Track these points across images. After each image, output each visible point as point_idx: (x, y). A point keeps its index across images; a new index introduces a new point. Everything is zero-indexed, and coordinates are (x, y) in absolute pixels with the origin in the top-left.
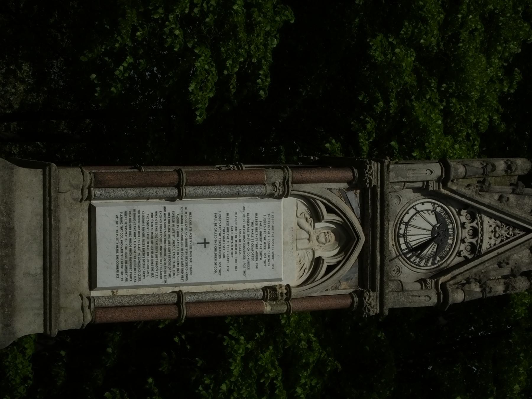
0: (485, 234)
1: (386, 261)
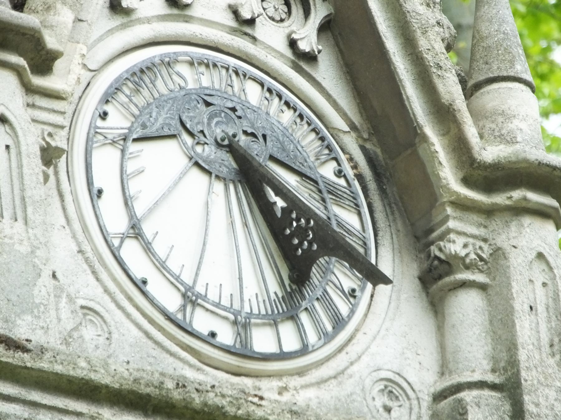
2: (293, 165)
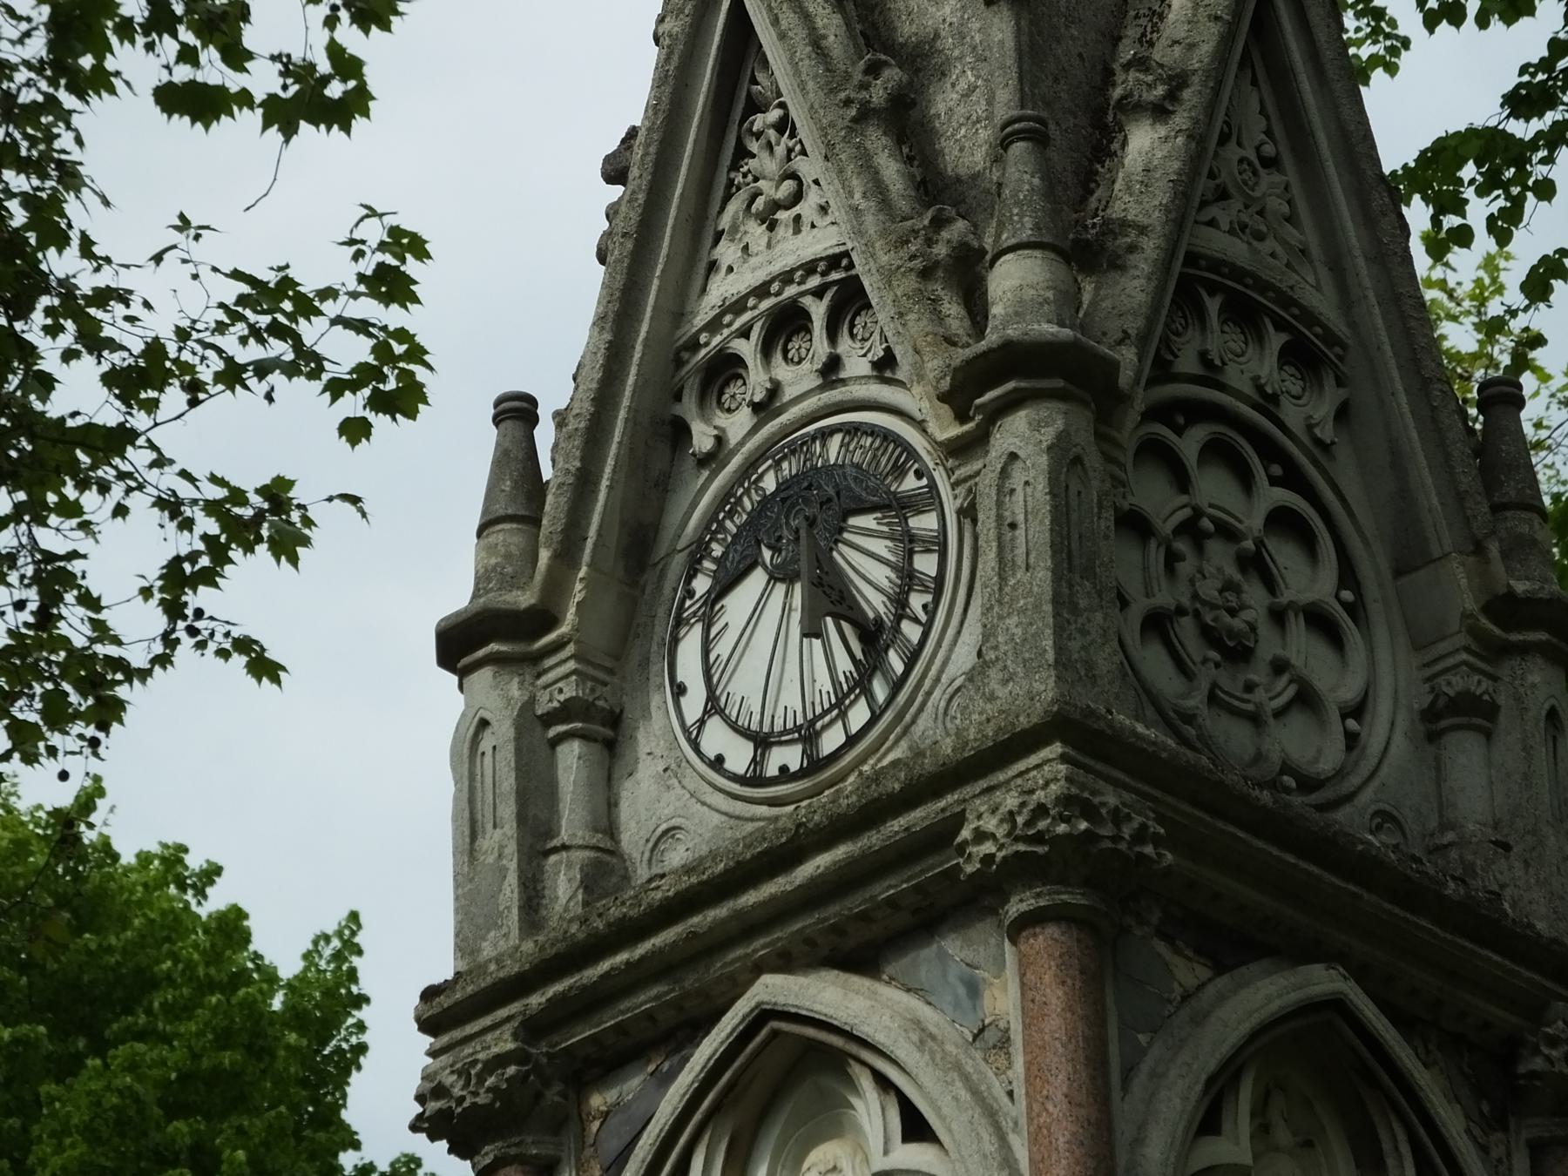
0: (778, 267)
2: (867, 505)
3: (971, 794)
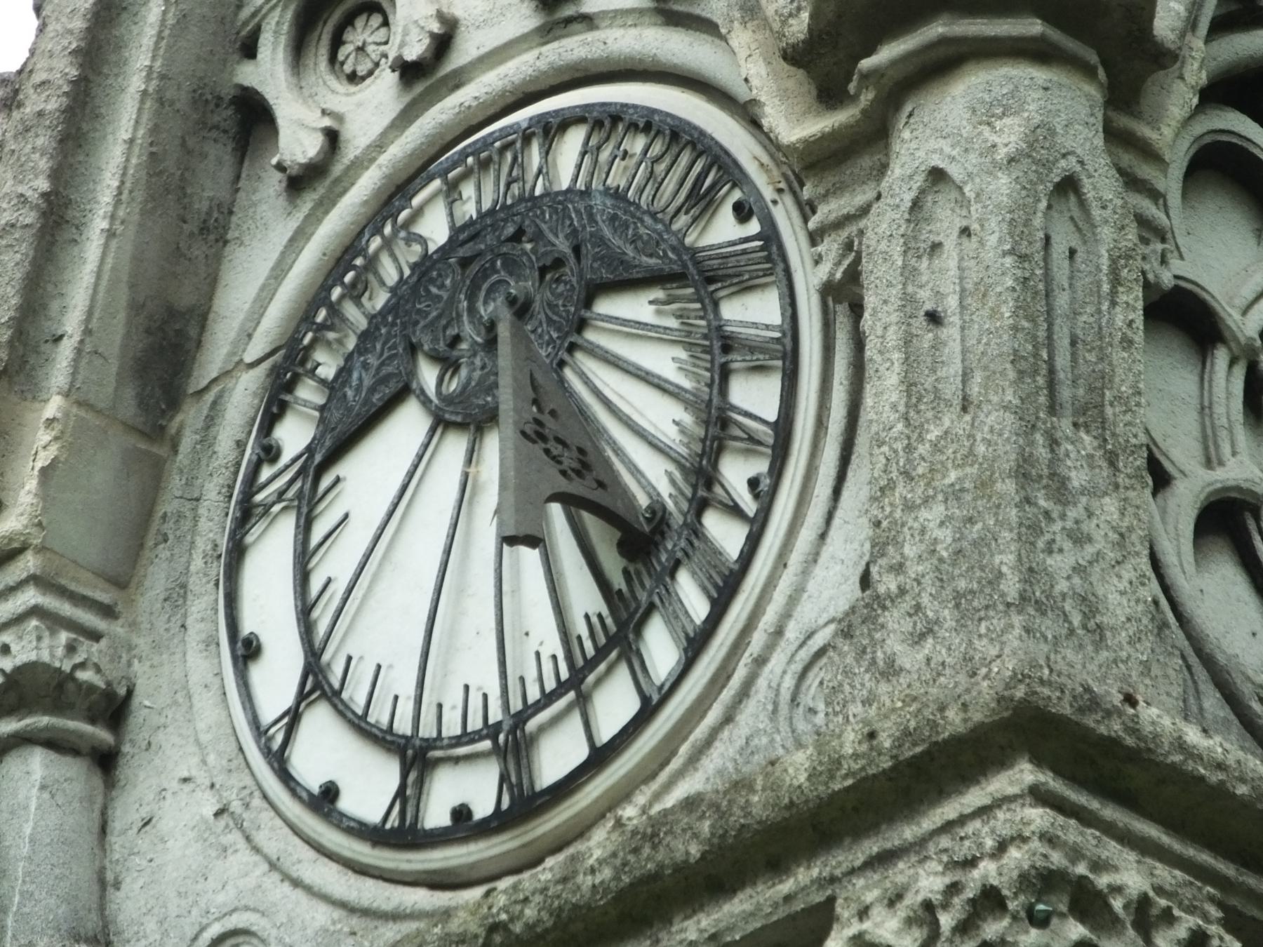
1: (530, 913)
3: (845, 867)
